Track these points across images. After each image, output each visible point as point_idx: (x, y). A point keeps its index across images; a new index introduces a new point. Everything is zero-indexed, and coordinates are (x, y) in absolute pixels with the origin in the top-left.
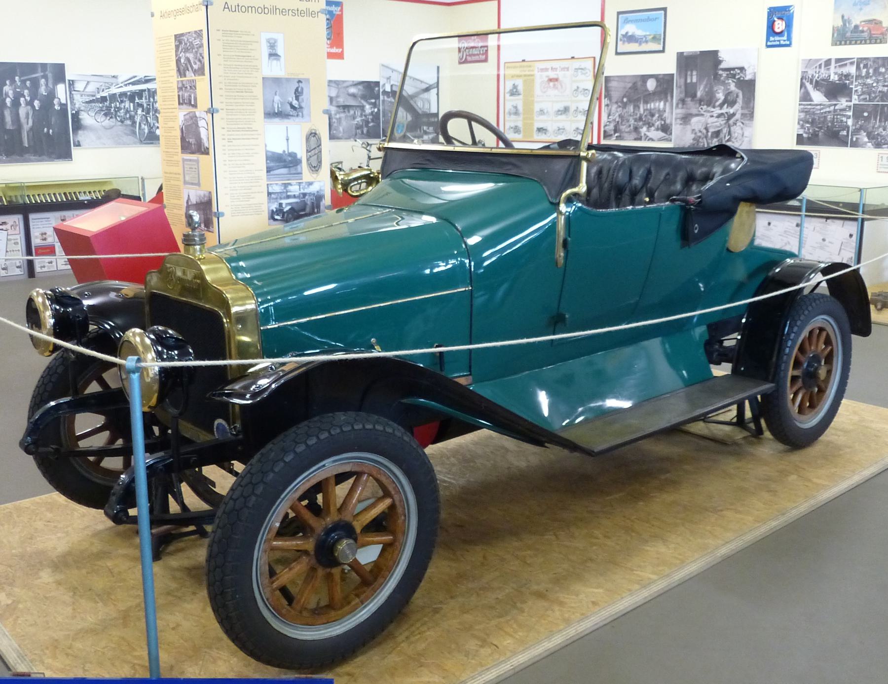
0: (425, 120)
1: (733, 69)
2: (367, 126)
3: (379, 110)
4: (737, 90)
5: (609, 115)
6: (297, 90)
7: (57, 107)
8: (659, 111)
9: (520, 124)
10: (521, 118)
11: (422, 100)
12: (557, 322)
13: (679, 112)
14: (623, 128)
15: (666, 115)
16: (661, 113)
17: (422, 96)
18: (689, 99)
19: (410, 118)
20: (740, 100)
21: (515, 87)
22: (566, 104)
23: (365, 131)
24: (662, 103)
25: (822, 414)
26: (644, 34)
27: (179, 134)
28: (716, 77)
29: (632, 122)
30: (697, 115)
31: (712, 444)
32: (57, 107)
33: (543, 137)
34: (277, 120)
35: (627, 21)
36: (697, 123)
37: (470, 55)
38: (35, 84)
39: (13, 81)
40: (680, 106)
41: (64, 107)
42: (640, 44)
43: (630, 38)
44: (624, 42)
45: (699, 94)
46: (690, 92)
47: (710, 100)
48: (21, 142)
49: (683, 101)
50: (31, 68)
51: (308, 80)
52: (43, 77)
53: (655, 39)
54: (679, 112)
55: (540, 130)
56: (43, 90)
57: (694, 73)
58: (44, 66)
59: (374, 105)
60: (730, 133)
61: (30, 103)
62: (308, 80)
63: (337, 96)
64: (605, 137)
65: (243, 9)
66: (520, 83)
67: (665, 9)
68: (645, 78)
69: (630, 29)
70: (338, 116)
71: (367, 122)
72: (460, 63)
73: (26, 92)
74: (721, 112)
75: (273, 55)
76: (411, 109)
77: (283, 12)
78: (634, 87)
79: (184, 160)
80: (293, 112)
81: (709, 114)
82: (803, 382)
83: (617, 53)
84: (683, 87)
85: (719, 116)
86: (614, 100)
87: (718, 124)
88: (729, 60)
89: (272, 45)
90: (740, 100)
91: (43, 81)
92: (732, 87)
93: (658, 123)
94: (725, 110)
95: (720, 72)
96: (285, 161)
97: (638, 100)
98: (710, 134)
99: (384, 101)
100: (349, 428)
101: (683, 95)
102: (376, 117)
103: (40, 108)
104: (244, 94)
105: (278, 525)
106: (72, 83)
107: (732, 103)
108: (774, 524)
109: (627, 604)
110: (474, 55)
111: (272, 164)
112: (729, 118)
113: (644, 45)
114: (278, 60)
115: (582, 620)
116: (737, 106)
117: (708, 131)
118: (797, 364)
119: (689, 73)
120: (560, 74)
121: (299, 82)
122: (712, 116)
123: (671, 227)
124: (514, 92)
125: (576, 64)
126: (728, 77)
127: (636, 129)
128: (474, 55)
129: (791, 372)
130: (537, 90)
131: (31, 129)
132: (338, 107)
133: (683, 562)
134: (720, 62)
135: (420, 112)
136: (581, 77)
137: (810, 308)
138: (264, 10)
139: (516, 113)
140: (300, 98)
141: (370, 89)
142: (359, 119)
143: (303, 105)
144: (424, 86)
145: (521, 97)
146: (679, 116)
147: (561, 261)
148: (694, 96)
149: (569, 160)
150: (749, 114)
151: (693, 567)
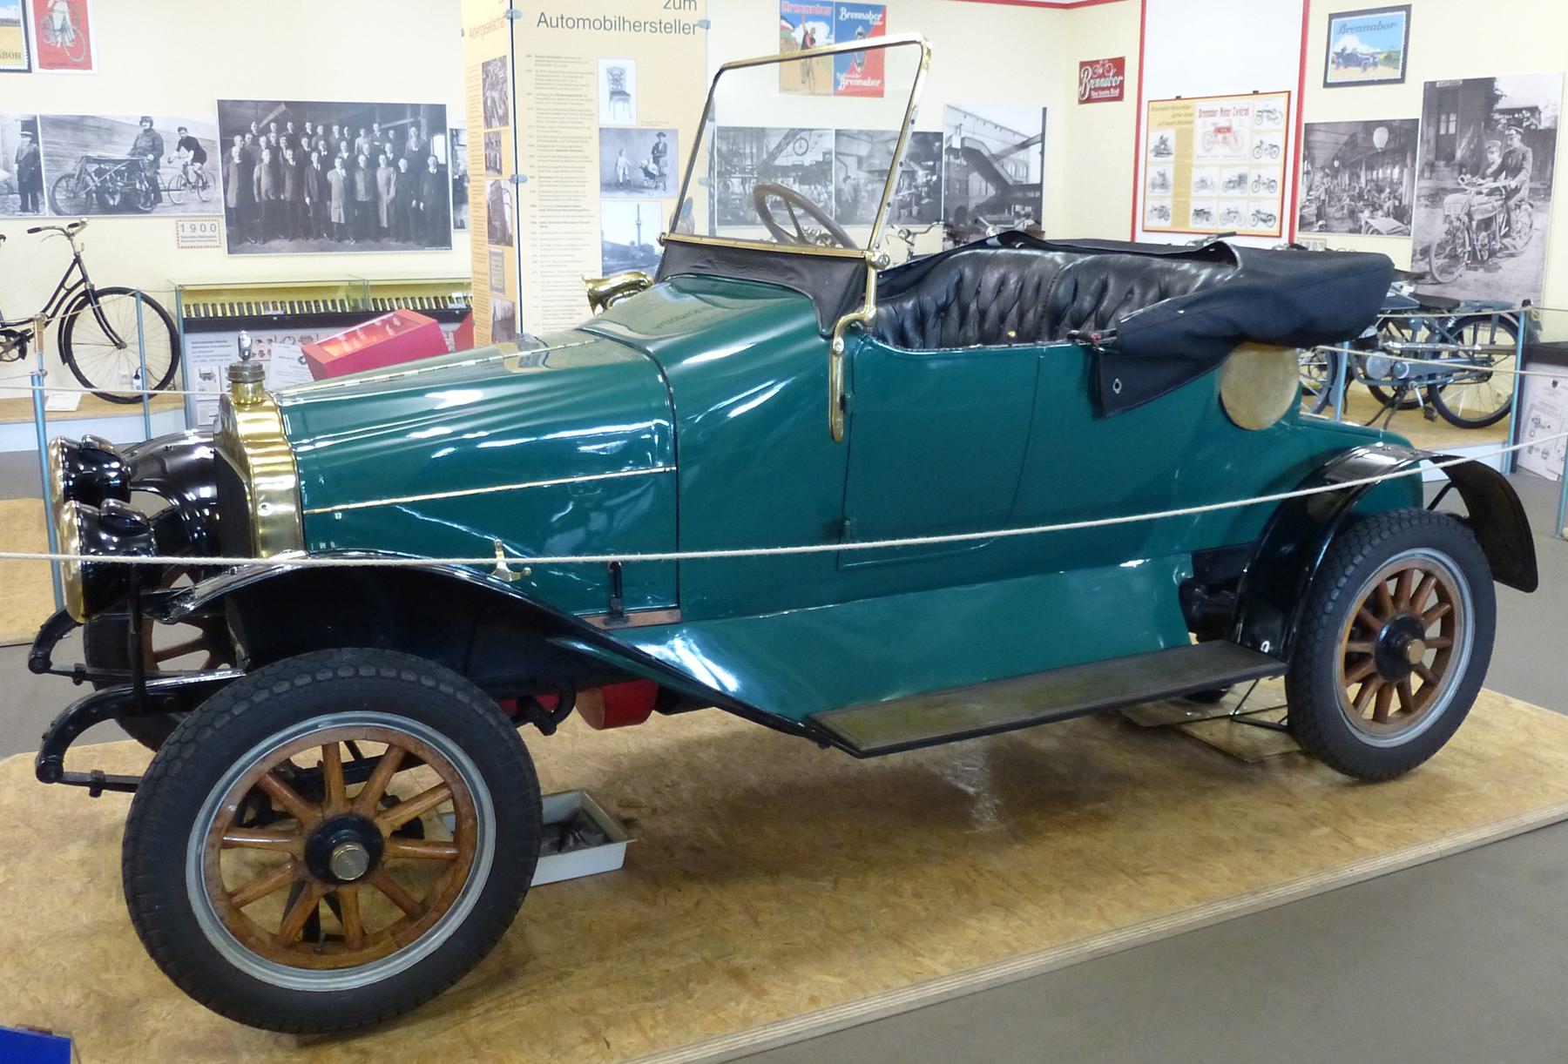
0: (1019, 195)
1: (1519, 110)
2: (918, 204)
3: (940, 178)
4: (1524, 148)
5: (1310, 189)
6: (656, 148)
7: (432, 170)
8: (1392, 181)
9: (1168, 203)
10: (1170, 193)
11: (1015, 162)
12: (837, 533)
13: (1424, 185)
14: (1331, 211)
15: (1402, 190)
16: (1395, 186)
17: (1013, 156)
18: (1442, 163)
19: (992, 191)
20: (1528, 165)
21: (1163, 141)
22: (1242, 170)
23: (915, 210)
24: (1397, 170)
25: (1425, 725)
26: (1372, 50)
27: (485, 213)
28: (1490, 124)
29: (1347, 201)
30: (1455, 191)
31: (1219, 760)
32: (432, 170)
33: (1203, 226)
34: (622, 194)
35: (1344, 30)
36: (1453, 204)
37: (1096, 89)
38: (402, 134)
39: (370, 131)
40: (1427, 174)
41: (442, 169)
42: (1365, 69)
43: (1348, 59)
44: (1338, 65)
45: (1459, 154)
46: (1443, 150)
47: (1476, 166)
48: (378, 220)
49: (1431, 167)
50: (392, 112)
51: (675, 132)
52: (413, 124)
53: (1390, 59)
54: (1424, 185)
55: (1199, 213)
56: (412, 144)
57: (1453, 117)
58: (415, 108)
59: (932, 170)
60: (1508, 223)
61: (393, 163)
62: (675, 132)
63: (871, 156)
64: (1301, 227)
65: (570, 23)
66: (1170, 134)
67: (1407, 8)
68: (1369, 127)
69: (1350, 43)
70: (869, 187)
71: (919, 198)
72: (1081, 102)
73: (388, 147)
74: (1495, 185)
75: (618, 94)
76: (994, 176)
77: (635, 26)
78: (1352, 143)
79: (491, 253)
80: (651, 183)
81: (1474, 189)
82: (1378, 664)
83: (1326, 85)
84: (1432, 142)
85: (1492, 192)
86: (1318, 164)
87: (1489, 206)
88: (1512, 94)
89: (616, 78)
90: (1528, 165)
91: (413, 131)
92: (1516, 142)
93: (1389, 204)
94: (1502, 182)
95: (1497, 116)
96: (633, 257)
97: (1357, 164)
98: (1474, 224)
99: (948, 164)
100: (351, 673)
101: (1431, 157)
102: (934, 189)
103: (408, 170)
104: (568, 154)
105: (233, 808)
106: (455, 134)
107: (1514, 171)
108: (1226, 907)
109: (867, 1010)
110: (1103, 89)
111: (612, 263)
112: (1508, 198)
113: (1370, 69)
114: (626, 101)
115: (773, 1023)
116: (1523, 176)
117: (1471, 219)
118: (1362, 630)
119: (1444, 117)
120: (1234, 121)
121: (660, 134)
122: (1480, 193)
123: (1070, 382)
124: (1162, 150)
125: (1260, 103)
126: (1508, 125)
127: (1353, 214)
128: (1103, 89)
129: (1342, 648)
130: (1198, 148)
131: (393, 201)
132: (871, 172)
133: (1014, 951)
134: (1497, 98)
135: (1010, 182)
136: (1267, 125)
137: (1386, 535)
138: (604, 24)
139: (1164, 185)
140: (662, 160)
141: (928, 145)
142: (905, 192)
143: (666, 171)
144: (1019, 140)
145: (1171, 158)
146: (1424, 192)
147: (840, 432)
148: (1450, 158)
149: (854, 265)
150: (1543, 191)
151: (1024, 965)
